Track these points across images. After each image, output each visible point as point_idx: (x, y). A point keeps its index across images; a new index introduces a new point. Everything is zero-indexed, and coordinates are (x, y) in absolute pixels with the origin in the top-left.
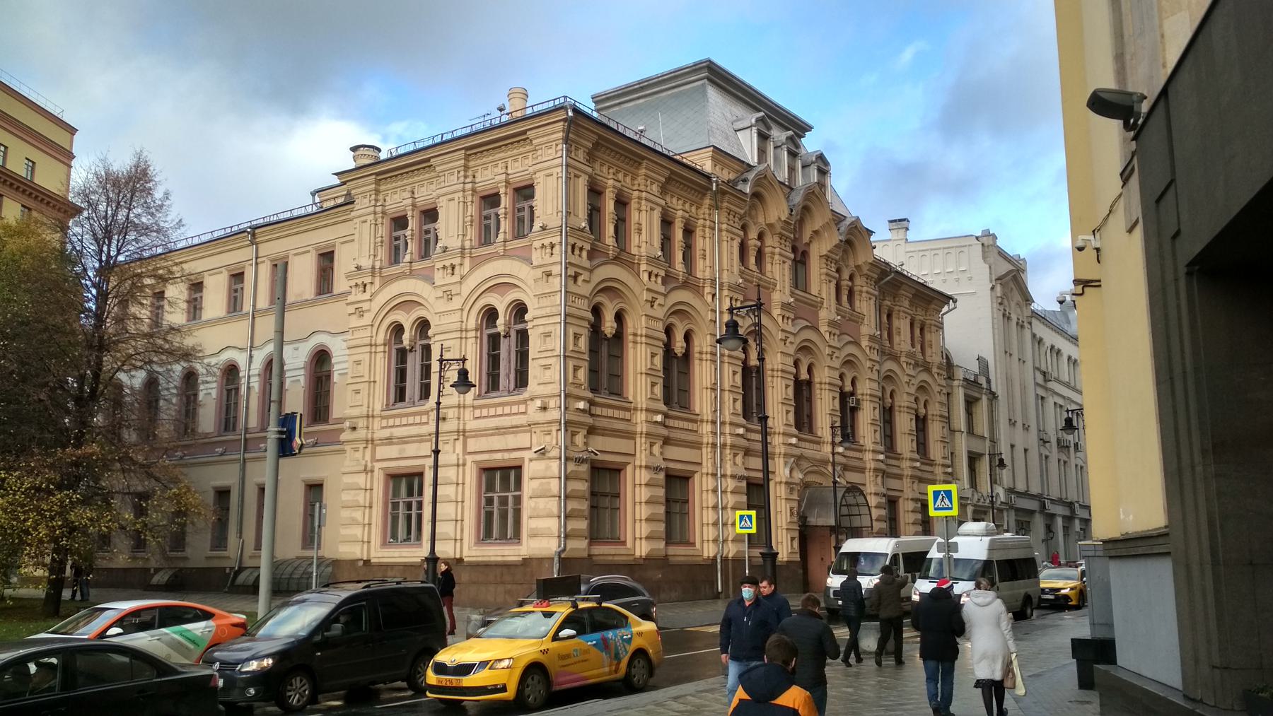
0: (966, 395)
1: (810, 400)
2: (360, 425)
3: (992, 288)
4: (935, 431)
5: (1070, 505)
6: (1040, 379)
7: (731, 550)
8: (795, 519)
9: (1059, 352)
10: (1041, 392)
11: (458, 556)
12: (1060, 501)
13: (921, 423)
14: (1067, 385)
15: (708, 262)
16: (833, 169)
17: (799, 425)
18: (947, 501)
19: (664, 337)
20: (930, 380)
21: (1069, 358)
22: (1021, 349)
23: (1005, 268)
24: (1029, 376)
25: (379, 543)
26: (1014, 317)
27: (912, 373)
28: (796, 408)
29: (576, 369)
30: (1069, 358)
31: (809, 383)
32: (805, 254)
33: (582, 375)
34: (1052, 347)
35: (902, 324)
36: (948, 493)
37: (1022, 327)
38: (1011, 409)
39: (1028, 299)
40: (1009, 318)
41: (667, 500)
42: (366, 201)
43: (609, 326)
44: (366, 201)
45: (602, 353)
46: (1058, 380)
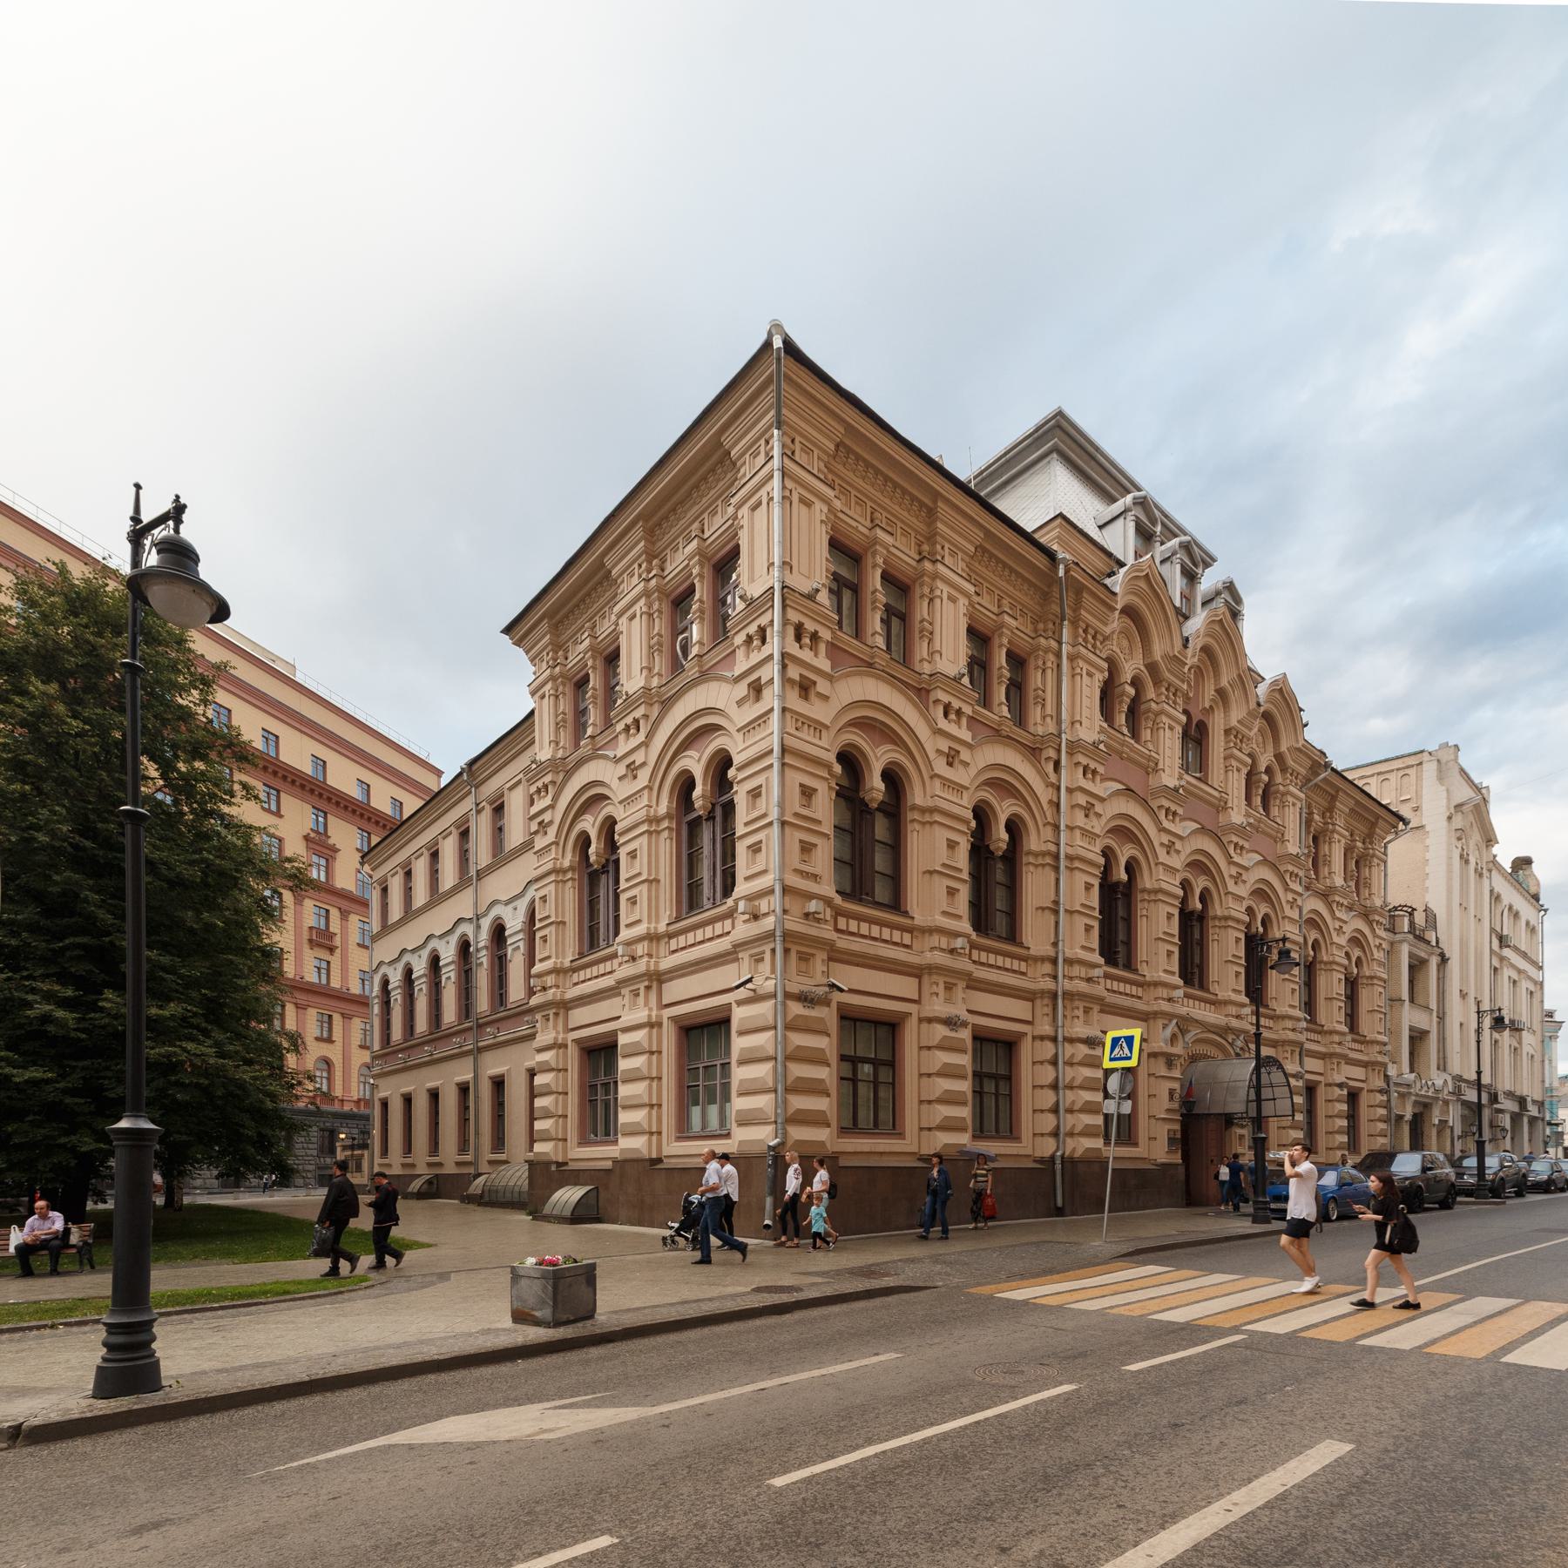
0: (1411, 955)
1: (1129, 921)
2: (640, 953)
3: (1450, 818)
4: (1369, 998)
5: (1522, 1101)
6: (1496, 943)
7: (1082, 1146)
8: (1176, 1106)
9: (1516, 915)
10: (1496, 963)
11: (654, 1156)
12: (1510, 1095)
13: (1352, 984)
14: (1524, 955)
15: (1049, 710)
16: (1248, 610)
17: (981, 918)
18: (1126, 1050)
19: (1181, 893)
20: (1367, 931)
21: (1528, 923)
22: (1478, 904)
23: (1464, 793)
24: (1486, 941)
25: (575, 1140)
26: (1472, 860)
27: (1344, 917)
28: (1102, 923)
29: (807, 848)
30: (1528, 923)
31: (1202, 917)
32: (1202, 728)
33: (824, 858)
34: (1510, 908)
35: (1336, 853)
36: (1130, 1040)
37: (1481, 875)
38: (1464, 978)
39: (1490, 840)
40: (1467, 862)
41: (976, 1074)
42: (635, 580)
43: (876, 786)
44: (635, 580)
45: (868, 824)
46: (1516, 949)
